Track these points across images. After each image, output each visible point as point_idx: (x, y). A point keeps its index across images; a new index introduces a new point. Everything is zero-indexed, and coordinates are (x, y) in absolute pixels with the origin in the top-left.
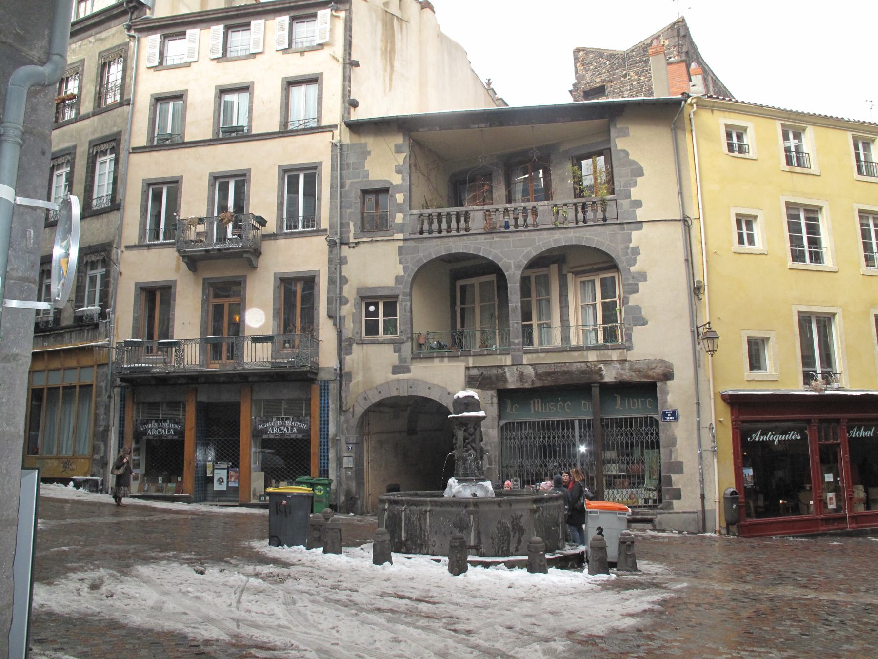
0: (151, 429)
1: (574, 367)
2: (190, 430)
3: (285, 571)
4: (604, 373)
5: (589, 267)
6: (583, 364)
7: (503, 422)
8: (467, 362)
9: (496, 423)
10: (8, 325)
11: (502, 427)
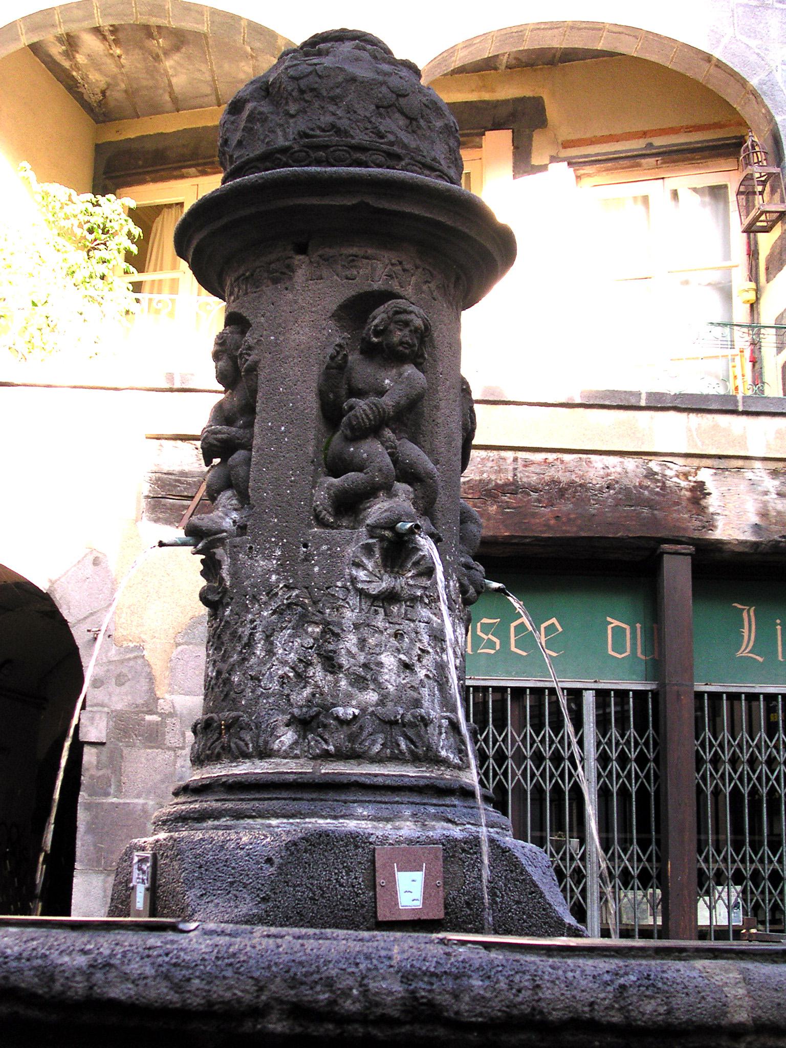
1: (598, 470)
2: (136, 728)
4: (713, 503)
5: (604, 157)
6: (631, 464)
10: (316, 569)
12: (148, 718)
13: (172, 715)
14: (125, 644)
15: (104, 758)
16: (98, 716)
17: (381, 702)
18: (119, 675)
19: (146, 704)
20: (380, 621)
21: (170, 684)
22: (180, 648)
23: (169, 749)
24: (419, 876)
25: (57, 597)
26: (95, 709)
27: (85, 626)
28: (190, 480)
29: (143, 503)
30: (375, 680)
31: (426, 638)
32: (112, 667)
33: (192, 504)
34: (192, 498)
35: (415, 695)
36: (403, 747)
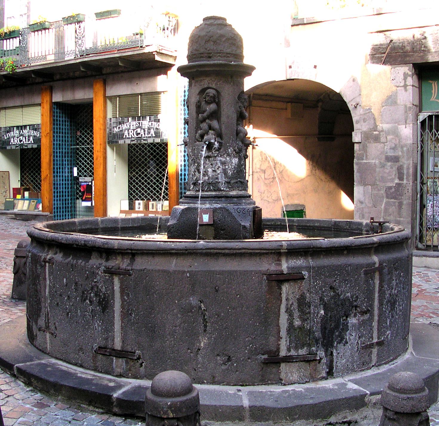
0: (14, 137)
3: (273, 169)
7: (423, 116)
8: (79, 38)
9: (411, 116)
11: (423, 123)
12: (375, 133)
13: (382, 131)
14: (365, 108)
15: (361, 147)
16: (358, 134)
17: (208, 179)
18: (364, 119)
19: (374, 128)
20: (207, 162)
21: (381, 121)
22: (384, 108)
23: (382, 143)
24: (208, 216)
25: (342, 94)
26: (357, 131)
27: (352, 103)
28: (383, 47)
29: (368, 57)
30: (207, 174)
31: (219, 164)
32: (362, 116)
33: (385, 55)
34: (385, 53)
35: (216, 177)
36: (212, 188)
